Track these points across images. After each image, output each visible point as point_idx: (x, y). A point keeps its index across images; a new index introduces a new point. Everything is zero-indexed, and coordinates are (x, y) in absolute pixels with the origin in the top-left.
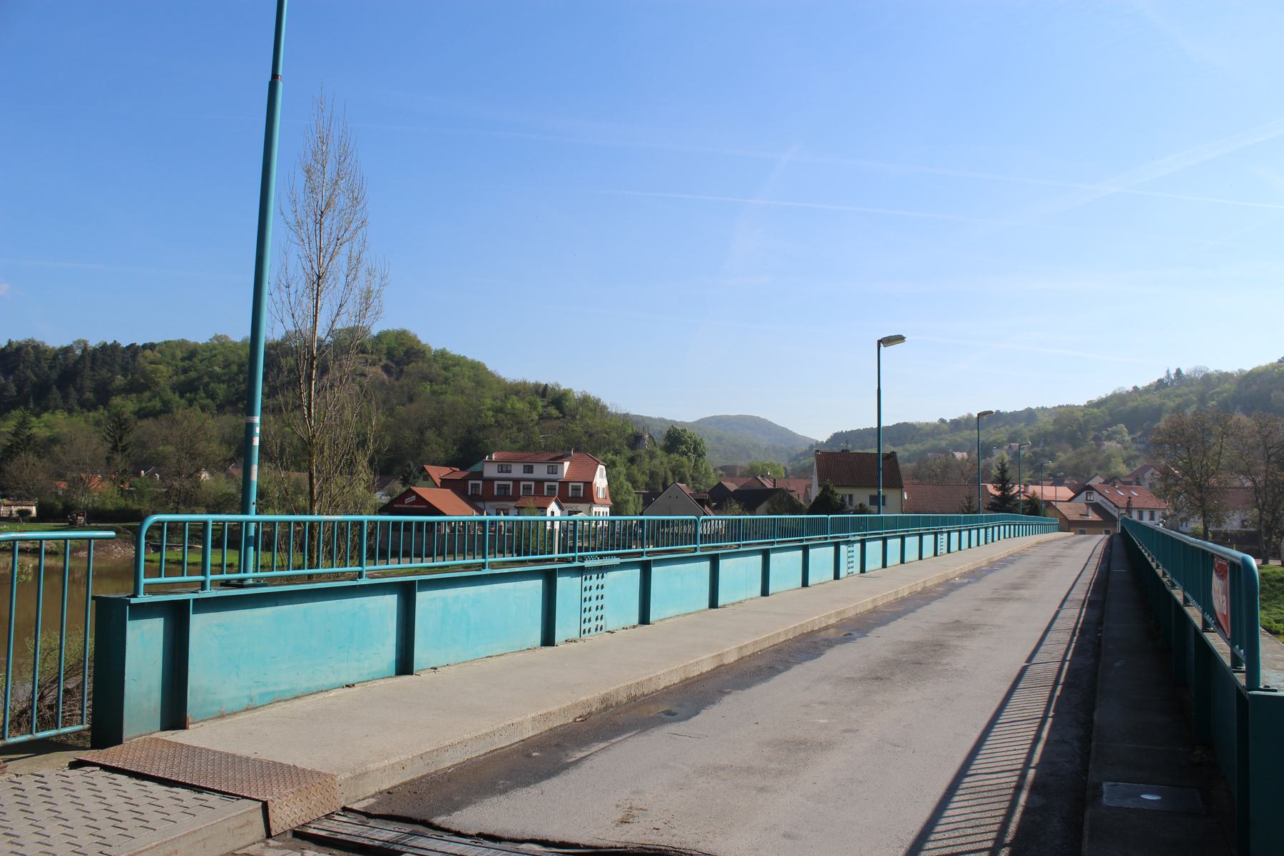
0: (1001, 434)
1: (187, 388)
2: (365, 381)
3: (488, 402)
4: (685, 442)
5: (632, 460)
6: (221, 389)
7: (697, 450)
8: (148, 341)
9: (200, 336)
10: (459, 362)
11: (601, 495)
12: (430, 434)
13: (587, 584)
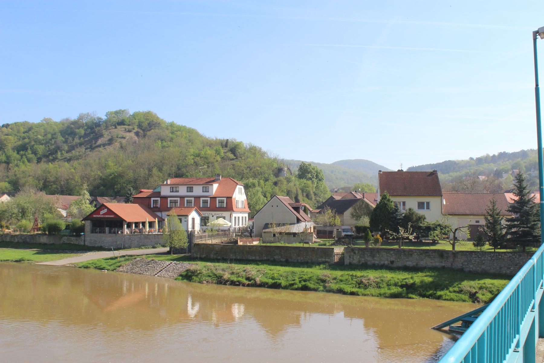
0: (507, 165)
1: (21, 149)
2: (124, 141)
3: (192, 151)
4: (310, 172)
5: (275, 184)
6: (41, 149)
7: (318, 177)
8: (5, 123)
9: (35, 118)
10: (181, 129)
11: (240, 206)
12: (155, 171)
13: (221, 272)
